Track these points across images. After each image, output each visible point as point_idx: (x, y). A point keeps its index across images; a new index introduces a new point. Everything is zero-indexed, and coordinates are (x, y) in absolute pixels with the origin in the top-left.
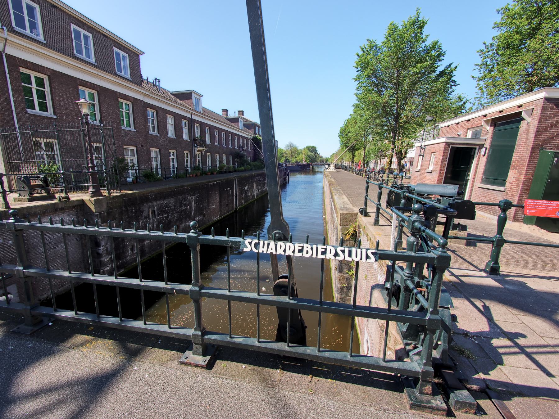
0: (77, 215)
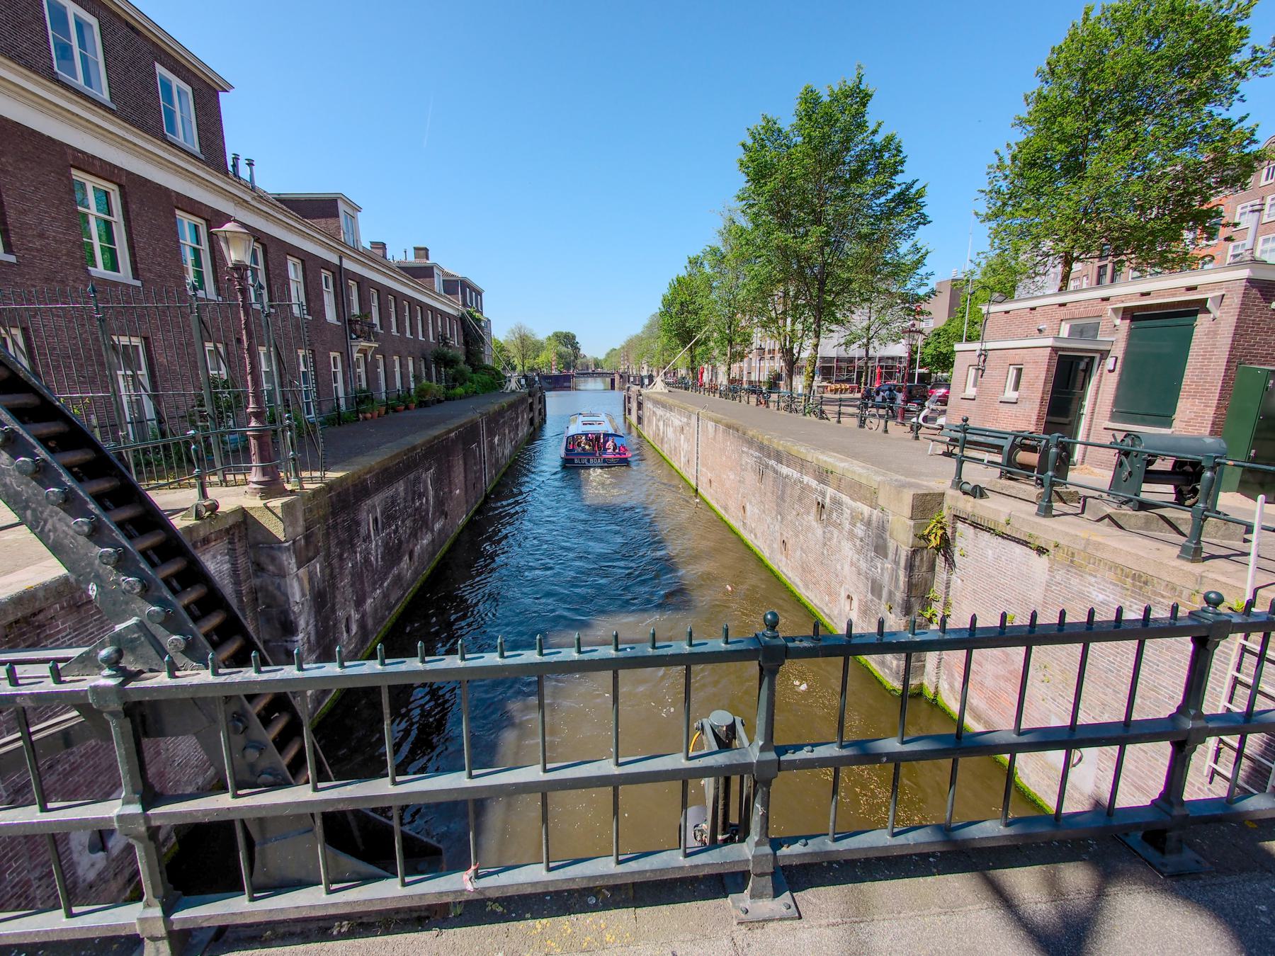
0: (232, 552)
